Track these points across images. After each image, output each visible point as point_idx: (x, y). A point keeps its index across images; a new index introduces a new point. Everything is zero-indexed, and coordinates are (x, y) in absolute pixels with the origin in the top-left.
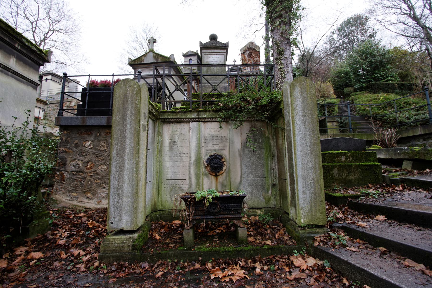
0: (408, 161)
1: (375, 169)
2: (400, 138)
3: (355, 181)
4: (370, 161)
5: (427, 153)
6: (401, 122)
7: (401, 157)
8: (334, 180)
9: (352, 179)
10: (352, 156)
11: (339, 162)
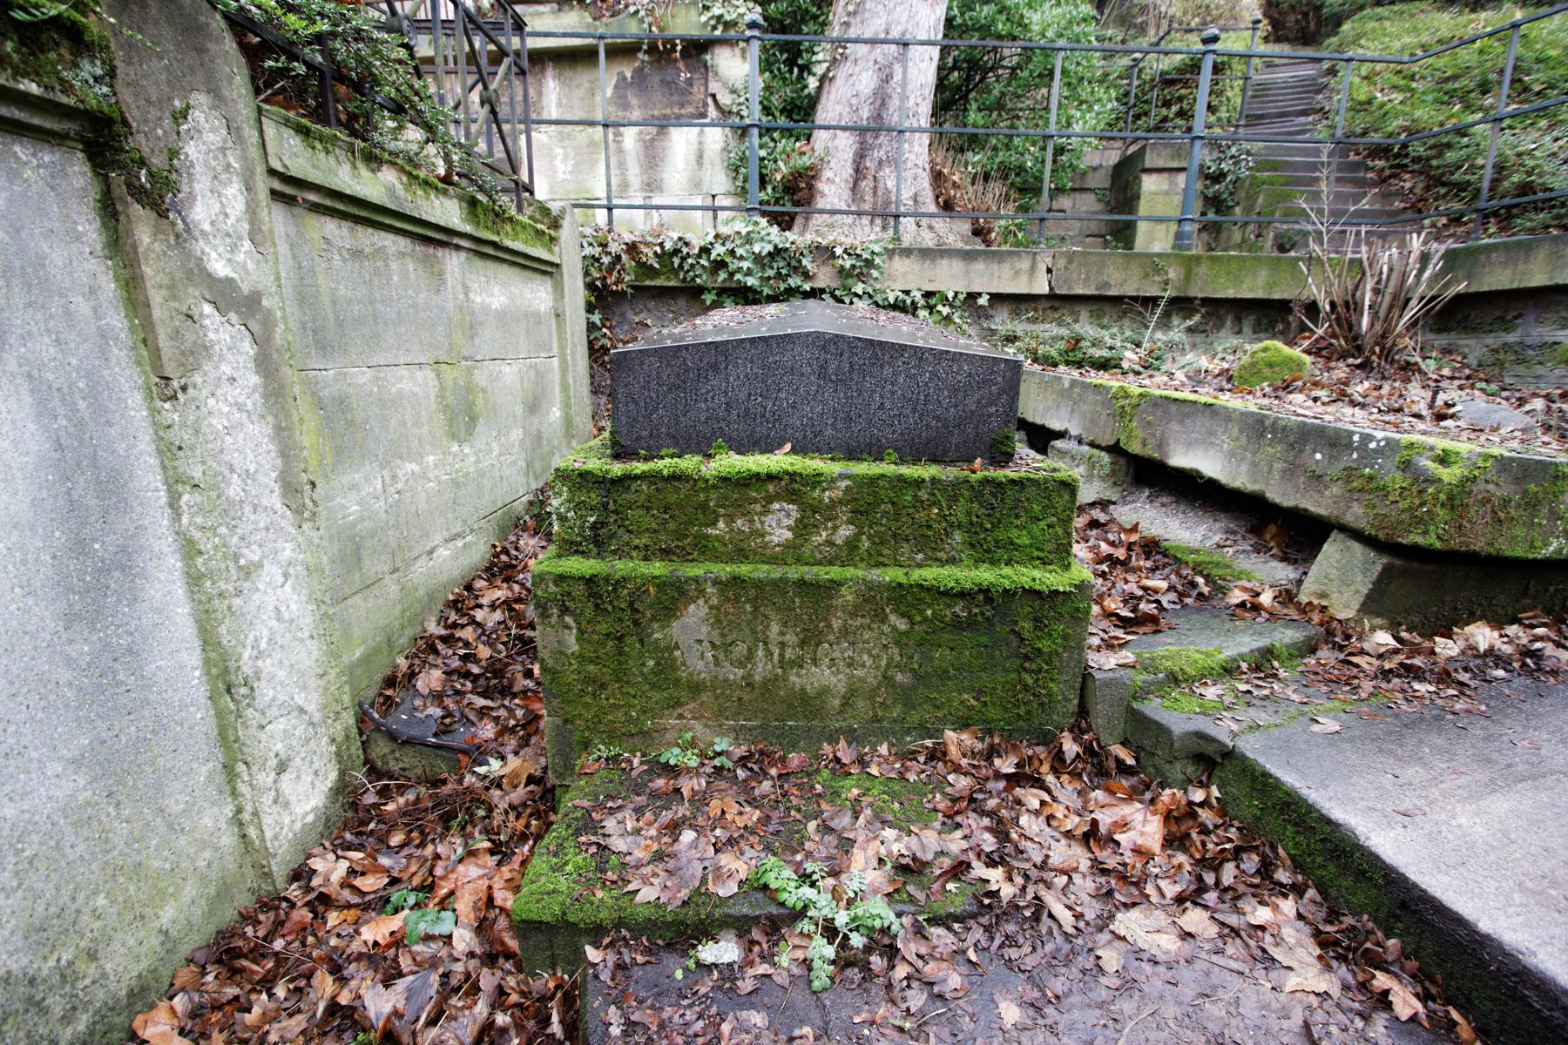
0: (1357, 548)
1: (1026, 626)
2: (1459, 299)
3: (847, 702)
4: (1008, 553)
5: (1532, 504)
6: (1525, 189)
7: (1317, 504)
8: (684, 694)
9: (825, 691)
10: (865, 501)
11: (741, 554)
